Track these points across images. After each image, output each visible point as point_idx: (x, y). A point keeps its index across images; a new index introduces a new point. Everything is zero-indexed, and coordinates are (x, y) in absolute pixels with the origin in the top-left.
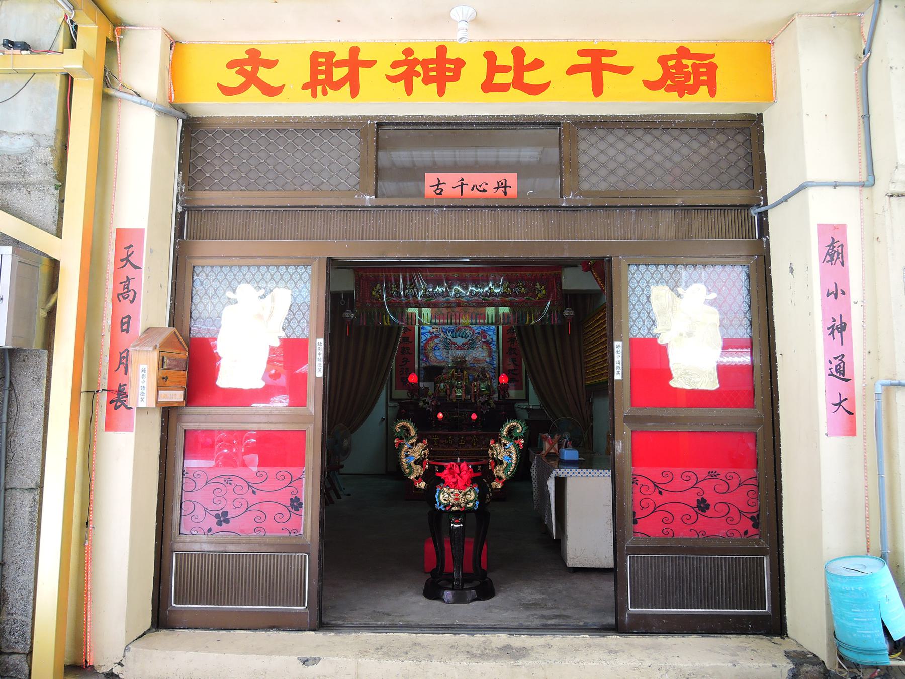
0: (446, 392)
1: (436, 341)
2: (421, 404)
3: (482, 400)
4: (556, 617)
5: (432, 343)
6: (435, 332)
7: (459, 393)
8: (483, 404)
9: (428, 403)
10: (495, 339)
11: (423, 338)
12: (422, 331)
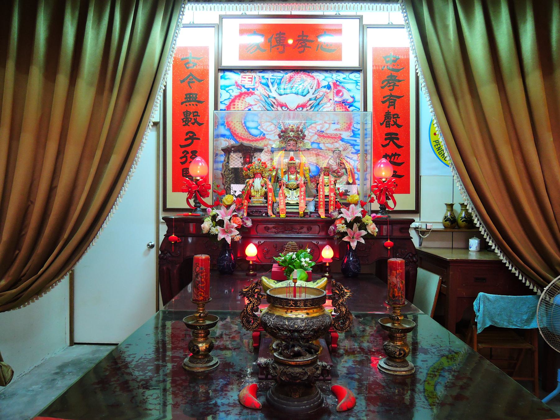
0: (266, 196)
1: (249, 100)
2: (207, 225)
3: (349, 215)
4: (396, 371)
5: (240, 105)
6: (248, 84)
7: (293, 197)
8: (350, 225)
9: (221, 223)
10: (359, 96)
11: (224, 96)
12: (222, 82)
